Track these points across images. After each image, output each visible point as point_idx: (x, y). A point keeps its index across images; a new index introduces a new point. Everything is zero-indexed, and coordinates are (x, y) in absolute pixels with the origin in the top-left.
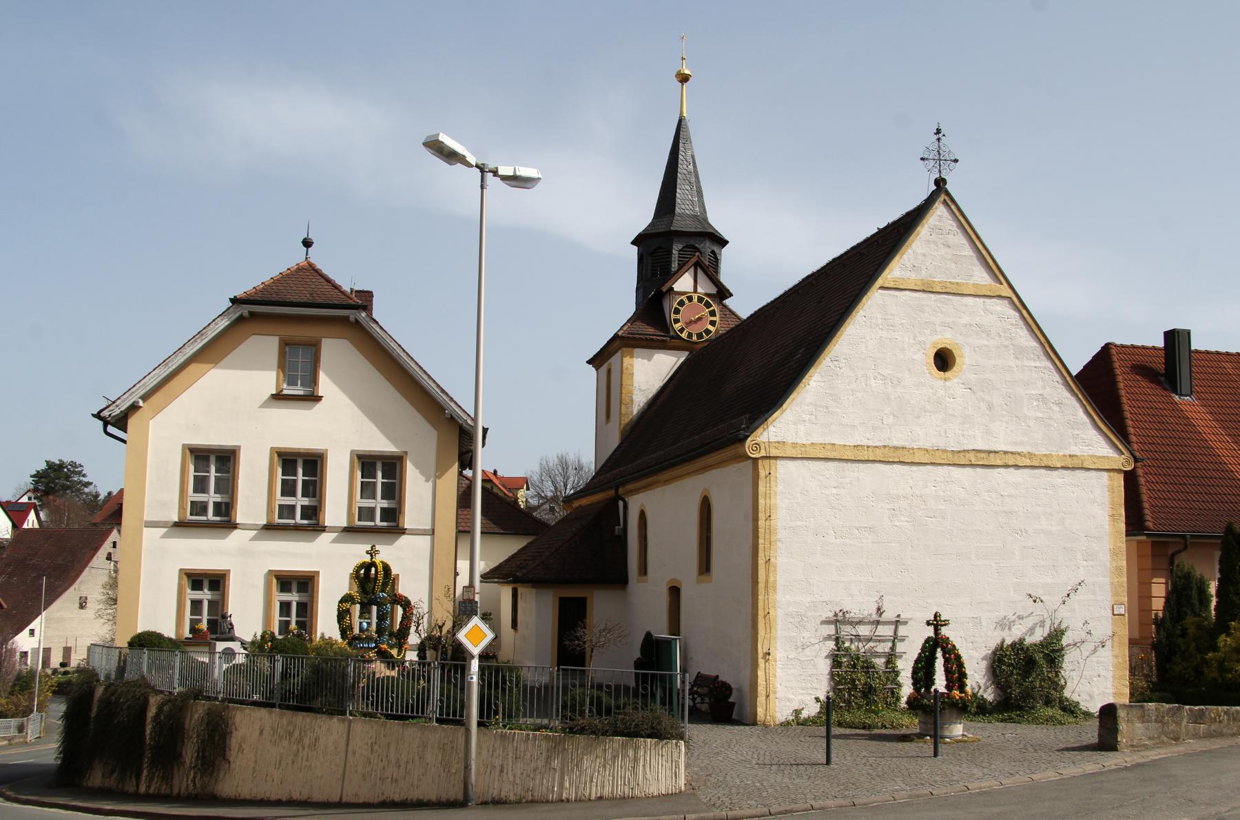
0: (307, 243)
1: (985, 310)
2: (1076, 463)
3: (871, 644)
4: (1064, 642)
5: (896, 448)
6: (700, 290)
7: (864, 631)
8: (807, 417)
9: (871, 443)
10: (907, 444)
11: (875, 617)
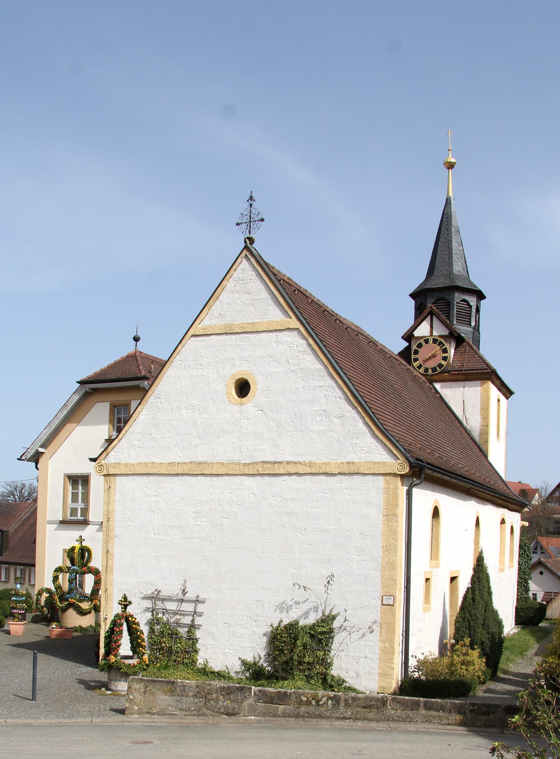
0: (136, 339)
1: (277, 342)
2: (353, 469)
3: (178, 617)
4: (336, 624)
5: (200, 463)
6: (435, 333)
7: (171, 606)
8: (136, 443)
9: (182, 460)
10: (209, 460)
11: (180, 596)
